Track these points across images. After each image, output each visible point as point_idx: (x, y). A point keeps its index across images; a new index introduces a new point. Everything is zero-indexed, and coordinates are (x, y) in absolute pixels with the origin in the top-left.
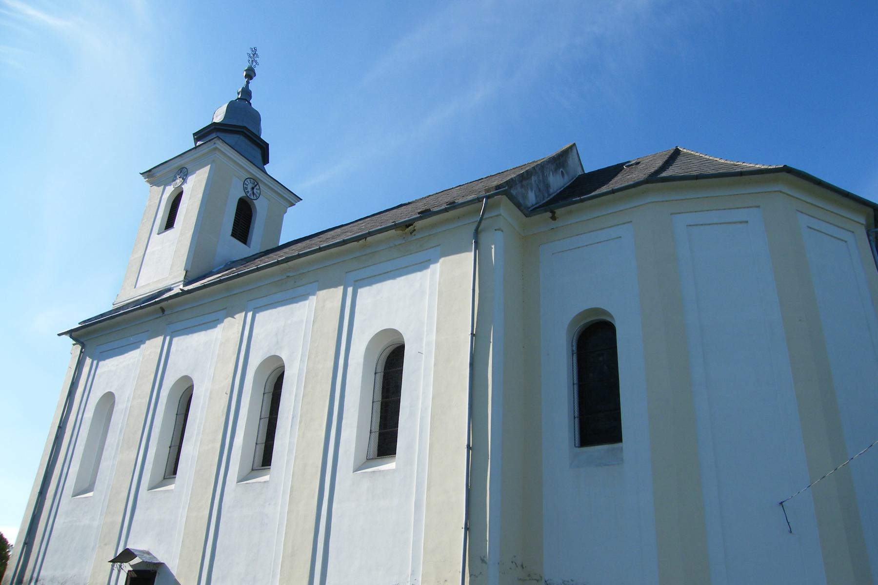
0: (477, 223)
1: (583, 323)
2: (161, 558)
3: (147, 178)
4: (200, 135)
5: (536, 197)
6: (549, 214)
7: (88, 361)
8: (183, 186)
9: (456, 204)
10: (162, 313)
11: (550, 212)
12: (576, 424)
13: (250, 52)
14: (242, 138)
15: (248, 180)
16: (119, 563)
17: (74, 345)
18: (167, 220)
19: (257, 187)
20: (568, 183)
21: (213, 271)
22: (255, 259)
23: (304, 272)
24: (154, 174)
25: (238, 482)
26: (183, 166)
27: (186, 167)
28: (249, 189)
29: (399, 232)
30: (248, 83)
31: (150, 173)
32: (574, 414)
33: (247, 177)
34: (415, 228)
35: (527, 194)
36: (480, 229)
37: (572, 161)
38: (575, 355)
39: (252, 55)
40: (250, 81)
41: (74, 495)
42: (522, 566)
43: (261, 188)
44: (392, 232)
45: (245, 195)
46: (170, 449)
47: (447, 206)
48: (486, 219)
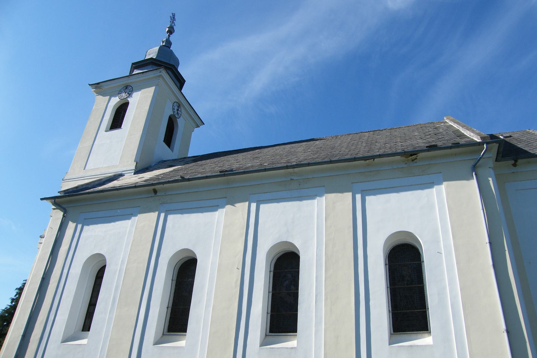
3: (95, 89)
7: (71, 226)
8: (129, 99)
9: (460, 145)
11: (514, 161)
15: (175, 103)
17: (54, 209)
18: (112, 121)
22: (296, 165)
23: (308, 178)
24: (101, 86)
25: (260, 346)
26: (128, 85)
27: (131, 85)
28: (176, 110)
29: (403, 158)
30: (169, 36)
31: (98, 85)
33: (175, 101)
36: (478, 164)
39: (172, 18)
41: (65, 341)
43: (182, 111)
44: (398, 158)
45: (172, 113)
46: (168, 309)
47: (452, 145)
48: (484, 158)
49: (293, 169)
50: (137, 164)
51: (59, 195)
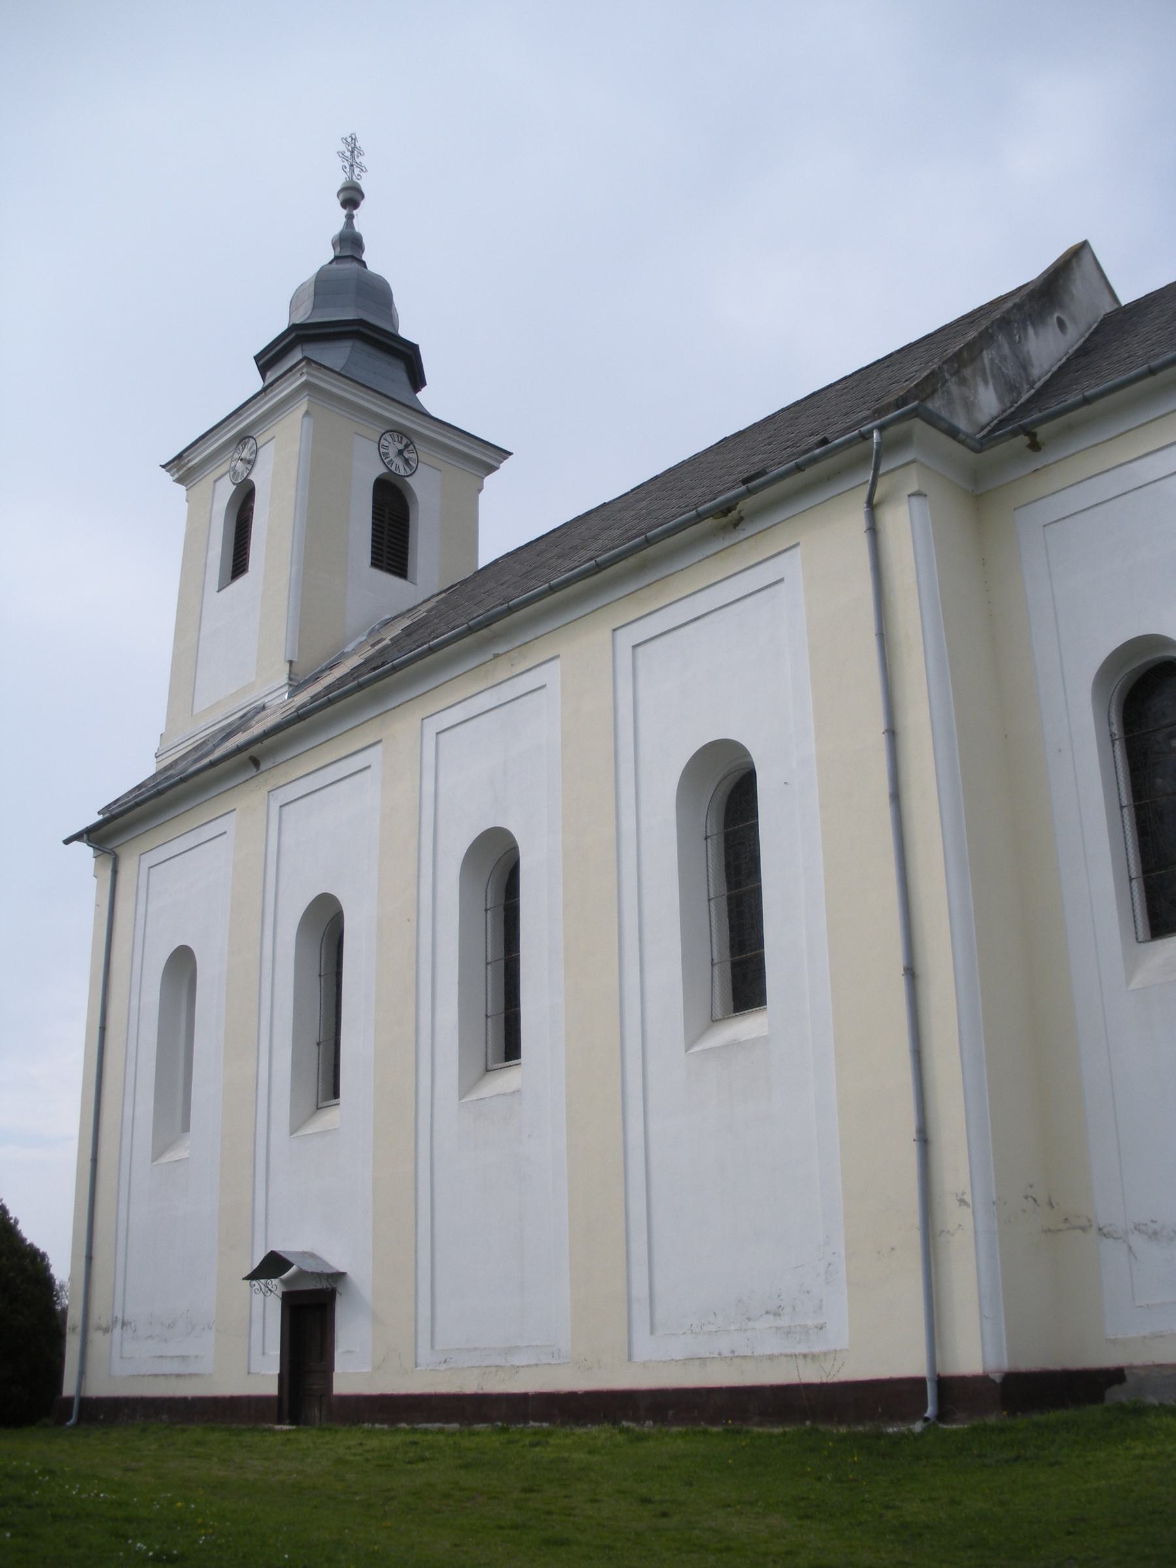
0: (868, 487)
1: (1136, 664)
2: (337, 1261)
4: (267, 360)
5: (1000, 398)
6: (1023, 440)
8: (251, 477)
10: (256, 770)
11: (1026, 435)
12: (1134, 894)
13: (343, 147)
14: (359, 345)
16: (263, 1281)
19: (411, 447)
20: (1078, 340)
21: (346, 650)
30: (350, 217)
32: (1129, 871)
33: (383, 431)
34: (743, 514)
35: (975, 398)
37: (1080, 287)
38: (1117, 743)
40: (355, 212)
42: (1051, 1205)
49: (488, 628)
50: (293, 664)
51: (101, 817)
